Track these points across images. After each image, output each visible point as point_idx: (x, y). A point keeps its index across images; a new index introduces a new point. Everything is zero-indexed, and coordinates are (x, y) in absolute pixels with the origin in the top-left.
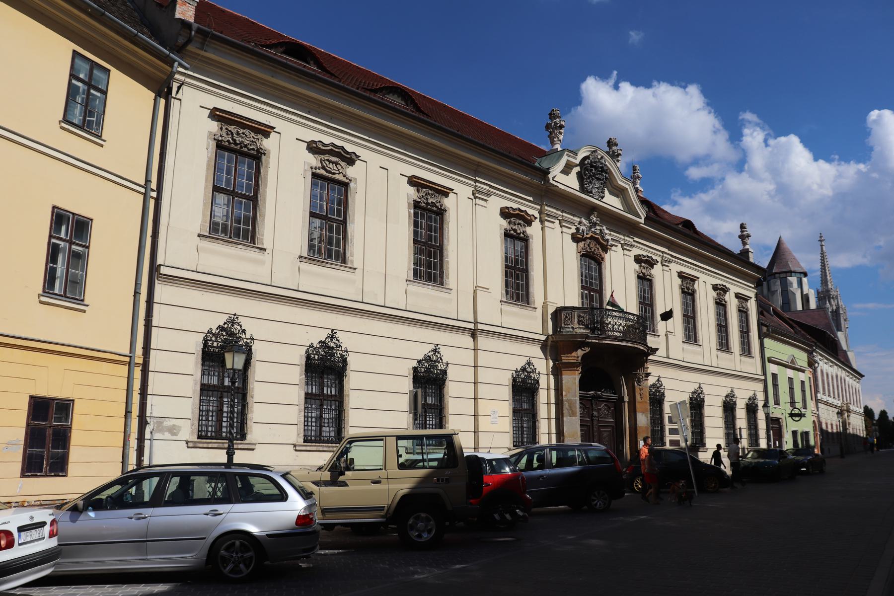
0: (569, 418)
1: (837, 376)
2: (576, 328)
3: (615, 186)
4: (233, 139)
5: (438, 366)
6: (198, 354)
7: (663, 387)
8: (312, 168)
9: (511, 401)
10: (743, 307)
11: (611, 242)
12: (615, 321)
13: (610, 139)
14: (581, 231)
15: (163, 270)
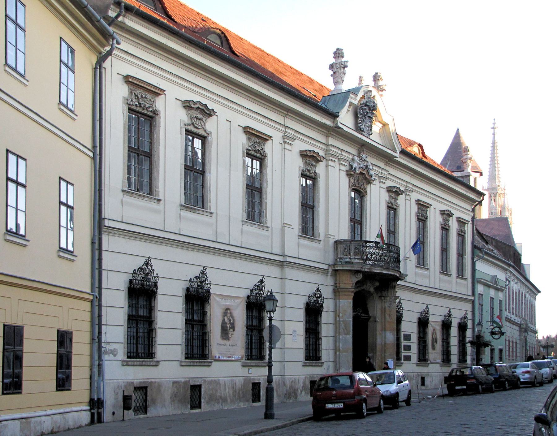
0: (344, 336)
1: (519, 291)
2: (352, 259)
4: (139, 103)
5: (150, 278)
6: (126, 290)
7: (402, 309)
8: (185, 125)
9: (304, 322)
10: (462, 231)
12: (373, 251)
13: (377, 73)
14: (354, 169)
15: (107, 223)
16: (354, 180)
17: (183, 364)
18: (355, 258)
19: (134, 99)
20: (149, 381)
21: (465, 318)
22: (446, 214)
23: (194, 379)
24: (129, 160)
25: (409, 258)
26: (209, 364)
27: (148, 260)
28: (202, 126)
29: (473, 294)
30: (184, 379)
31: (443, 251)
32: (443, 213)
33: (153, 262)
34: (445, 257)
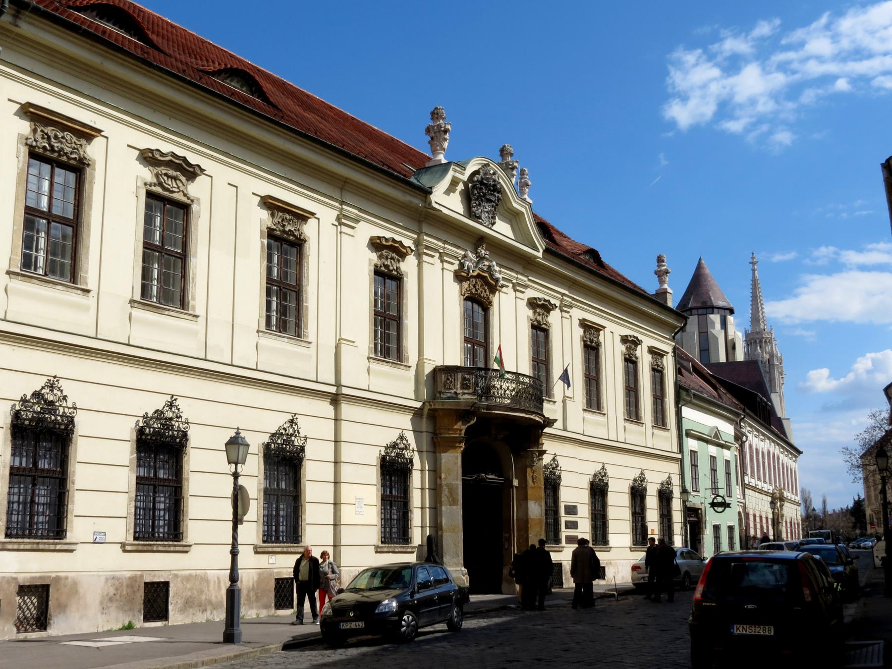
1: (769, 453)
3: (508, 208)
5: (294, 441)
7: (559, 468)
8: (145, 184)
10: (658, 365)
11: (502, 282)
14: (466, 268)
16: (469, 285)
17: (633, 549)
18: (464, 394)
19: (40, 140)
20: (54, 575)
21: (669, 482)
22: (631, 343)
23: (153, 573)
24: (376, 325)
25: (571, 398)
26: (186, 549)
27: (53, 381)
28: (178, 188)
29: (681, 450)
30: (132, 573)
31: (656, 399)
32: (625, 340)
33: (179, 402)
34: (633, 400)
